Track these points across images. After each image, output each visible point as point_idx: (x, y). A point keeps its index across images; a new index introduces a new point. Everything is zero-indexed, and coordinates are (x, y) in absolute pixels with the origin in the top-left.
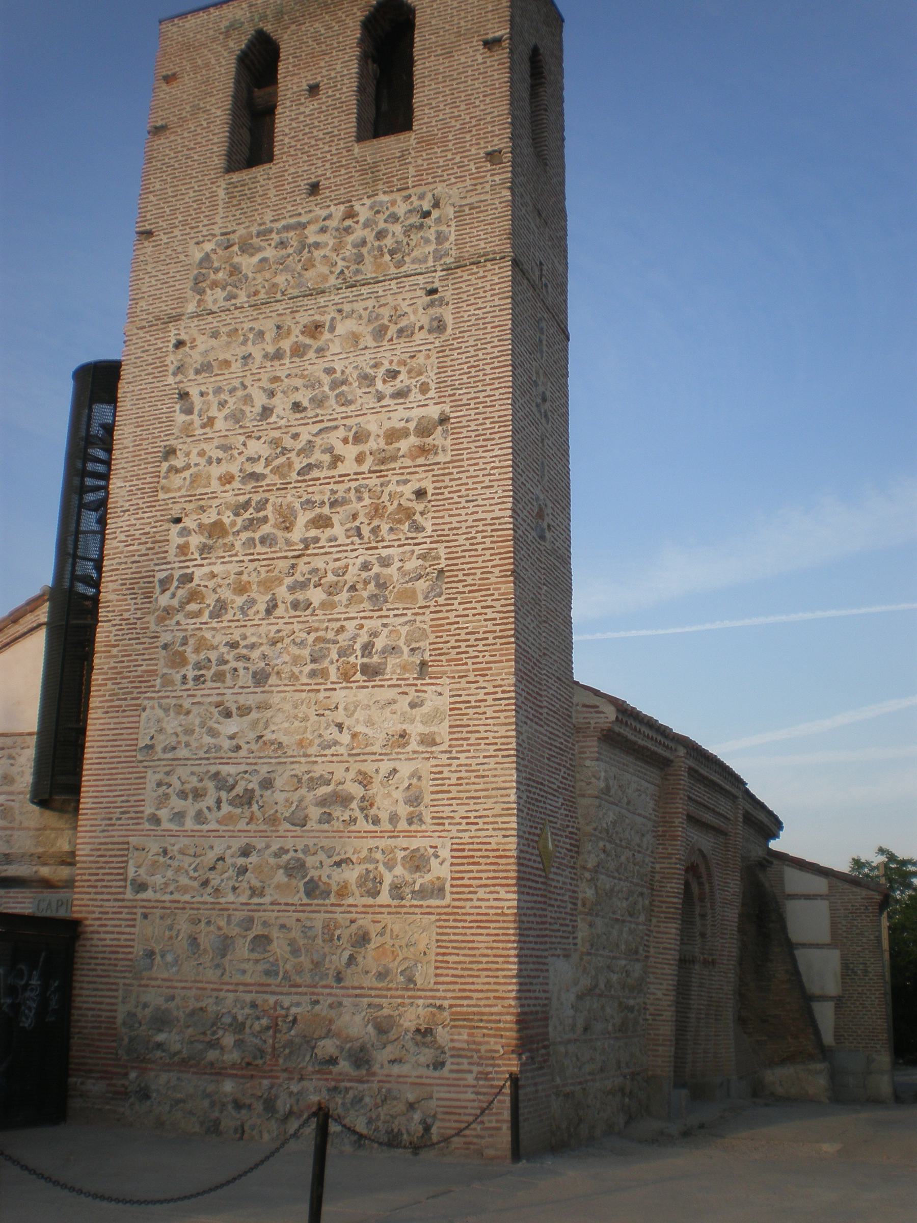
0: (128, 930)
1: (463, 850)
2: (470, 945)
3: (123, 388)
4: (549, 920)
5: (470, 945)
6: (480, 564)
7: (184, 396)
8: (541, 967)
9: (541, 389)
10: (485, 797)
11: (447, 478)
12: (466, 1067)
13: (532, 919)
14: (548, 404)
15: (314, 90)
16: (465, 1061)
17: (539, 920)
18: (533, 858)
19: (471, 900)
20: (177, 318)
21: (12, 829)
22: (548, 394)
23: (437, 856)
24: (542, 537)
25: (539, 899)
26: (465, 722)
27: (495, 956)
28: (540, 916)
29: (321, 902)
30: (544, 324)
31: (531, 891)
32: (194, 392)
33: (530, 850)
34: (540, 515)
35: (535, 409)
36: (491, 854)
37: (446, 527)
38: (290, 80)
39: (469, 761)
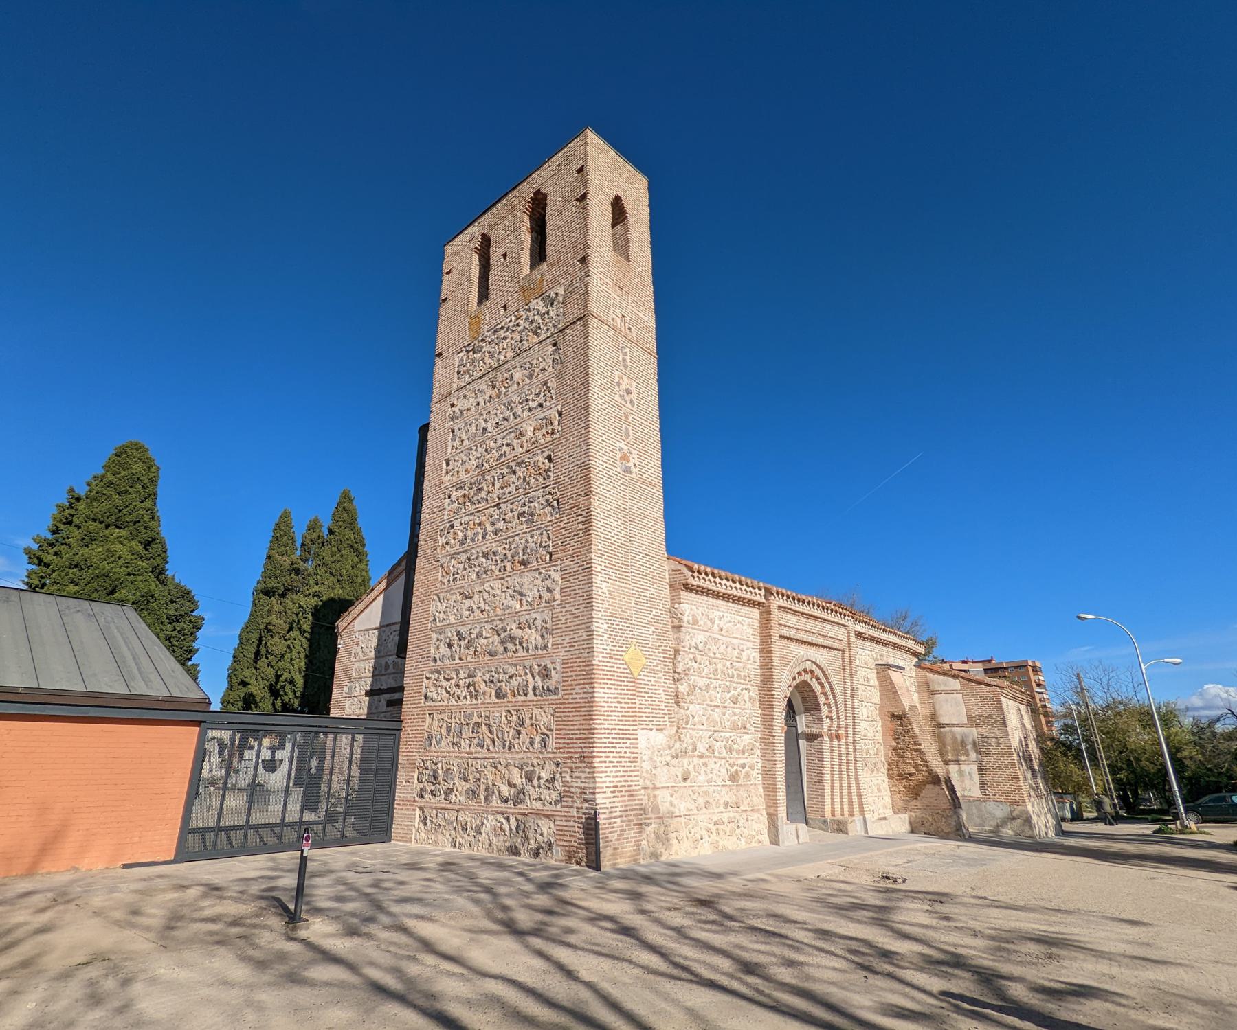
7: (453, 431)
15: (505, 256)
20: (449, 394)
32: (456, 429)
38: (495, 255)
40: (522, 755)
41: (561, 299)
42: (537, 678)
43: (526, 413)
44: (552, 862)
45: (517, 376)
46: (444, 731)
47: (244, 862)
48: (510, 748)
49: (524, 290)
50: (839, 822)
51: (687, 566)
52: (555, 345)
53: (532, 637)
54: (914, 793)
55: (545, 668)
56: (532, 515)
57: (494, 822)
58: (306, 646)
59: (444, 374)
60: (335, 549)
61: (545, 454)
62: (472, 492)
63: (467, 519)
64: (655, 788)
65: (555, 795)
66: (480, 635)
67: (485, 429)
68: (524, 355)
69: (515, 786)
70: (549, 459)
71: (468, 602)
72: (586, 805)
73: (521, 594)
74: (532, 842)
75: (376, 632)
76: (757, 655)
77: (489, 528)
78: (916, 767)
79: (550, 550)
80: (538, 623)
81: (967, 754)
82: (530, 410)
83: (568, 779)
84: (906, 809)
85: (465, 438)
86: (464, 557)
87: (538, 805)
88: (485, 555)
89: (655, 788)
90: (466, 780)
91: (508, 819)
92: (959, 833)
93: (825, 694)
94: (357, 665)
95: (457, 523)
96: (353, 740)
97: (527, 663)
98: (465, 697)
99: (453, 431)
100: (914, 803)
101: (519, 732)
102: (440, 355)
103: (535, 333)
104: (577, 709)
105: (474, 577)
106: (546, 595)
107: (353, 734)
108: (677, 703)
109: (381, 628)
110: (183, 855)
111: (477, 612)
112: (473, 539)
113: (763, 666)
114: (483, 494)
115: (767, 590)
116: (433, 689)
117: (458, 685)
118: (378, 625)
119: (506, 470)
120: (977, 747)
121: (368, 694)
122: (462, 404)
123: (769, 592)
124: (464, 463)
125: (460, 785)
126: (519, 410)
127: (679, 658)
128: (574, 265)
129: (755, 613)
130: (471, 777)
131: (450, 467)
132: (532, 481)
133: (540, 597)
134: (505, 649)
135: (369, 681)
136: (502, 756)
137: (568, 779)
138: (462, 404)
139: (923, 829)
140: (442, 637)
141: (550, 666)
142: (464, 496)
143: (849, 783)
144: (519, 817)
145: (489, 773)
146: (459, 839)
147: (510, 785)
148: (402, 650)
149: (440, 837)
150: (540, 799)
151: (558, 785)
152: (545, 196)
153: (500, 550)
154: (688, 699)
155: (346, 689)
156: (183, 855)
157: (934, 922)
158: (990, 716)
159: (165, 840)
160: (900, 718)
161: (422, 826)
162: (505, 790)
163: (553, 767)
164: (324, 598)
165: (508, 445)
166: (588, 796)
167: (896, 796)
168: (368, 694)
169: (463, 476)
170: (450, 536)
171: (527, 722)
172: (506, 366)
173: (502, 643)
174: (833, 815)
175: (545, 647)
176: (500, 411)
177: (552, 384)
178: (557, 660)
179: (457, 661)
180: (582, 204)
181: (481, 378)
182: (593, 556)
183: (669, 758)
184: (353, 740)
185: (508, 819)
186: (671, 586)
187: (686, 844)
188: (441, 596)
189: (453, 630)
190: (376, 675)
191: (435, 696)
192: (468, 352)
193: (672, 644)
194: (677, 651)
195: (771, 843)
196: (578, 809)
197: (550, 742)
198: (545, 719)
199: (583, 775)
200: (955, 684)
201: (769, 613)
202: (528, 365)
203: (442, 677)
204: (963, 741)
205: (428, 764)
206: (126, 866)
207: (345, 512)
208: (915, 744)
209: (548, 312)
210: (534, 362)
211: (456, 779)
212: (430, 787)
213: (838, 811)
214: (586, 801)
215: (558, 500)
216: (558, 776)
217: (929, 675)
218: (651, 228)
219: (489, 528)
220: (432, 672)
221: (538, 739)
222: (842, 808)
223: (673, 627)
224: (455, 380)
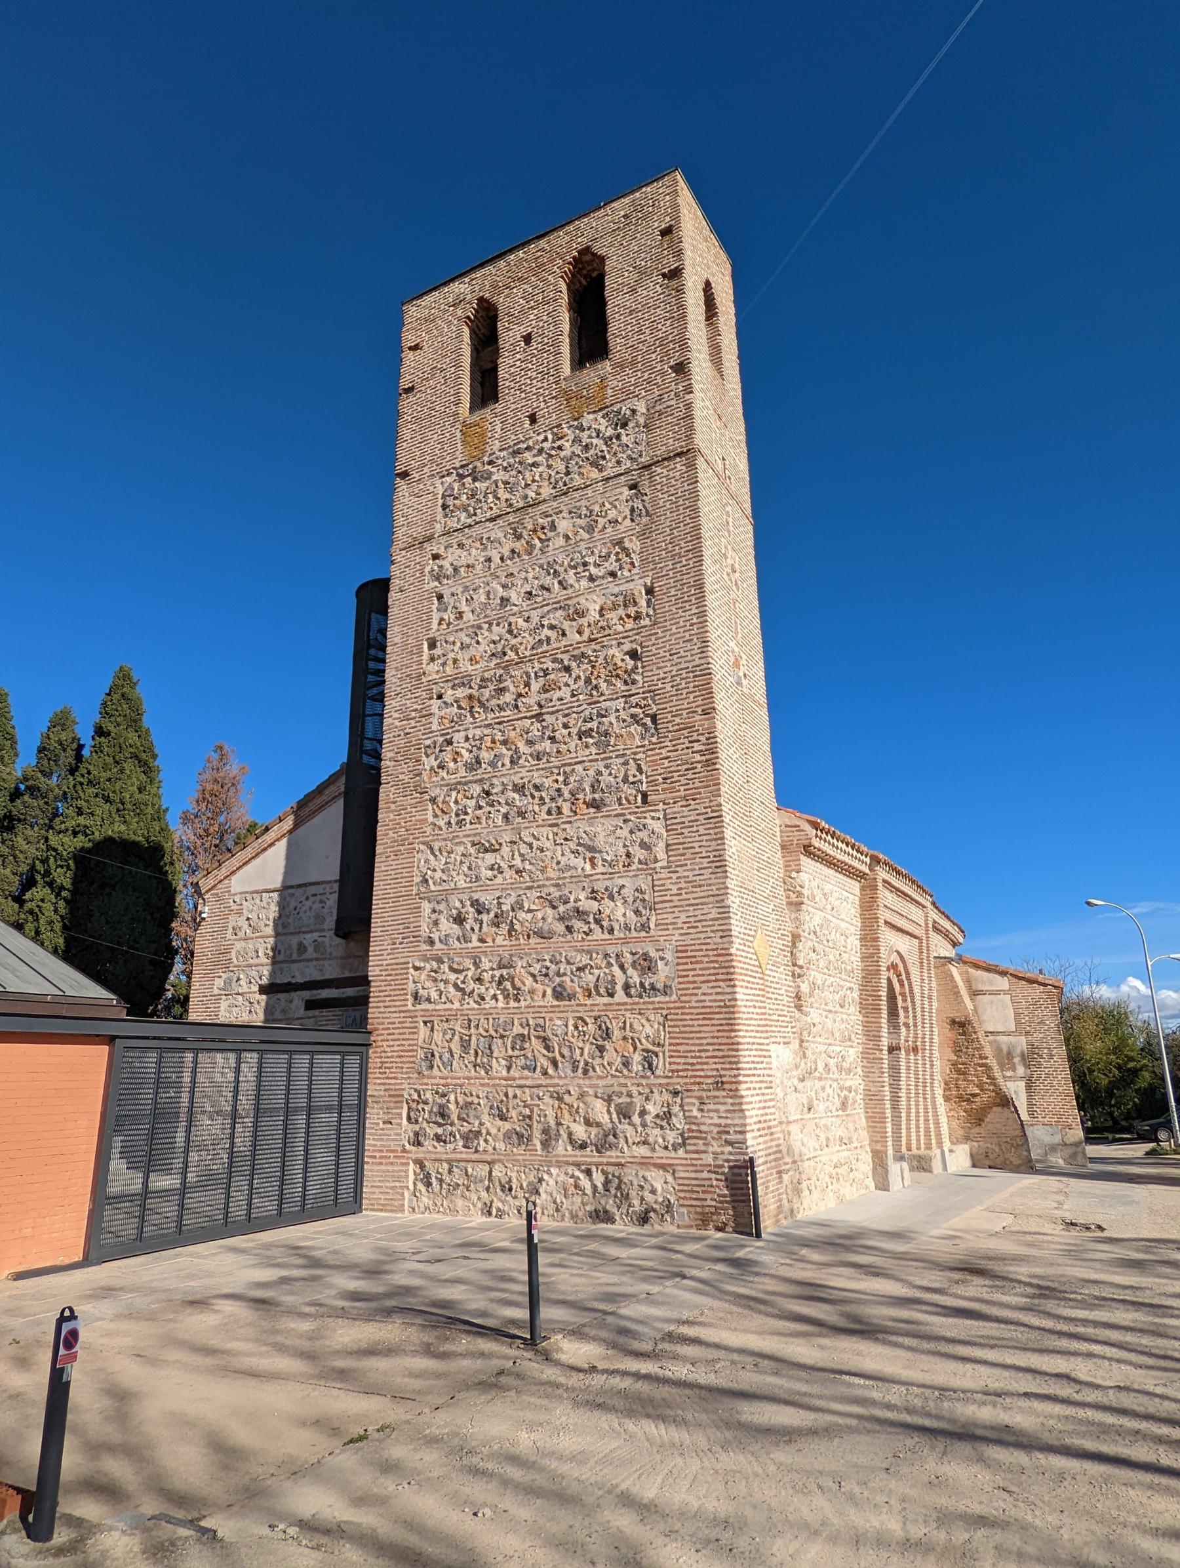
0: (411, 1036)
1: (687, 951)
2: (698, 1035)
3: (393, 596)
4: (768, 1011)
5: (698, 1035)
6: (686, 706)
7: (440, 597)
8: (764, 1053)
9: (730, 562)
10: (702, 904)
11: (653, 638)
12: (702, 1148)
13: (751, 1010)
14: (737, 575)
15: (528, 339)
16: (701, 1142)
17: (759, 1011)
18: (750, 956)
19: (696, 995)
20: (429, 539)
21: (324, 959)
22: (737, 566)
23: (662, 959)
24: (739, 683)
25: (757, 992)
26: (682, 841)
27: (720, 1044)
28: (760, 1008)
29: (567, 1003)
30: (729, 509)
31: (750, 985)
32: (446, 593)
33: (746, 949)
34: (737, 665)
35: (725, 577)
36: (711, 953)
37: (655, 678)
38: (509, 335)
39: (686, 874)
40: (609, 1081)
41: (642, 420)
42: (630, 971)
43: (584, 583)
44: (673, 1229)
45: (563, 525)
46: (455, 1046)
47: (197, 1256)
48: (585, 1072)
49: (568, 396)
50: (920, 1158)
51: (809, 821)
52: (633, 487)
53: (618, 912)
54: (977, 1118)
55: (646, 957)
56: (606, 734)
57: (562, 1178)
58: (63, 911)
59: (412, 506)
60: (110, 760)
61: (627, 647)
62: (486, 693)
63: (478, 732)
64: (789, 1122)
65: (672, 1137)
66: (518, 906)
67: (505, 601)
68: (577, 495)
69: (598, 1125)
70: (633, 655)
71: (490, 858)
72: (730, 1149)
73: (591, 849)
74: (636, 1202)
75: (275, 895)
76: (858, 943)
77: (523, 748)
78: (980, 1086)
79: (644, 787)
80: (628, 892)
81: (1014, 1069)
82: (592, 579)
83: (695, 1113)
84: (967, 1139)
85: (464, 607)
86: (476, 789)
87: (643, 1151)
88: (519, 789)
89: (789, 1122)
90: (503, 1118)
91: (588, 1173)
92: (1029, 1167)
93: (903, 995)
94: (239, 946)
95: (458, 737)
96: (239, 1062)
97: (611, 950)
98: (495, 997)
99: (440, 597)
100: (977, 1130)
101: (601, 1049)
102: (404, 475)
103: (595, 464)
104: (707, 1016)
105: (499, 820)
106: (639, 853)
107: (239, 1051)
108: (799, 1008)
109: (286, 890)
110: (96, 1252)
111: (508, 873)
112: (493, 764)
113: (864, 958)
114: (508, 698)
115: (873, 858)
116: (428, 984)
117: (479, 980)
118: (278, 884)
119: (550, 665)
120: (1027, 1060)
121: (263, 990)
122: (452, 557)
123: (875, 860)
124: (463, 647)
125: (491, 1125)
126: (571, 578)
127: (800, 946)
128: (663, 373)
129: (855, 886)
130: (513, 1113)
131: (438, 651)
132: (604, 685)
133: (628, 855)
134: (569, 929)
135: (266, 971)
136: (565, 1078)
137: (695, 1113)
138: (452, 557)
139: (988, 1162)
140: (442, 907)
141: (653, 954)
142: (470, 697)
143: (926, 1108)
144: (610, 1169)
145: (548, 1107)
146: (497, 1204)
147: (588, 1123)
148: (354, 921)
149: (460, 1203)
150: (645, 1143)
151: (678, 1122)
152: (602, 259)
153: (547, 782)
154: (810, 1000)
155: (219, 983)
156: (96, 1252)
157: (490, 1283)
158: (1042, 1022)
159: (68, 1232)
160: (962, 1025)
161: (421, 1186)
162: (580, 1131)
163: (667, 1097)
164: (97, 836)
165: (552, 627)
166: (733, 1136)
167: (955, 1123)
168: (263, 990)
169: (466, 667)
170: (447, 757)
171: (617, 1034)
172: (543, 507)
173: (562, 919)
174: (909, 1149)
175: (645, 927)
176: (534, 577)
177: (633, 545)
178: (665, 947)
179: (475, 943)
180: (674, 283)
181: (491, 520)
182: (722, 800)
183: (796, 1081)
184: (239, 1062)
185: (588, 1173)
186: (783, 847)
187: (816, 1195)
188: (436, 847)
189: (465, 897)
190: (278, 958)
191: (434, 995)
192: (461, 477)
193: (789, 926)
194: (796, 938)
195: (877, 1188)
196: (716, 1153)
197: (660, 1063)
198: (647, 1029)
199: (722, 1108)
200: (1003, 983)
201: (875, 888)
202: (584, 511)
203: (445, 967)
204: (1009, 1053)
205: (429, 1095)
206: (19, 1276)
207: (121, 703)
208: (981, 1057)
209: (618, 437)
210: (597, 508)
211: (485, 1118)
212: (432, 1130)
213: (914, 1146)
214: (729, 1143)
215: (654, 718)
216: (676, 1109)
217: (972, 971)
218: (738, 334)
219: (523, 748)
220: (426, 959)
221: (637, 1058)
222: (918, 1140)
223: (790, 904)
224: (439, 517)
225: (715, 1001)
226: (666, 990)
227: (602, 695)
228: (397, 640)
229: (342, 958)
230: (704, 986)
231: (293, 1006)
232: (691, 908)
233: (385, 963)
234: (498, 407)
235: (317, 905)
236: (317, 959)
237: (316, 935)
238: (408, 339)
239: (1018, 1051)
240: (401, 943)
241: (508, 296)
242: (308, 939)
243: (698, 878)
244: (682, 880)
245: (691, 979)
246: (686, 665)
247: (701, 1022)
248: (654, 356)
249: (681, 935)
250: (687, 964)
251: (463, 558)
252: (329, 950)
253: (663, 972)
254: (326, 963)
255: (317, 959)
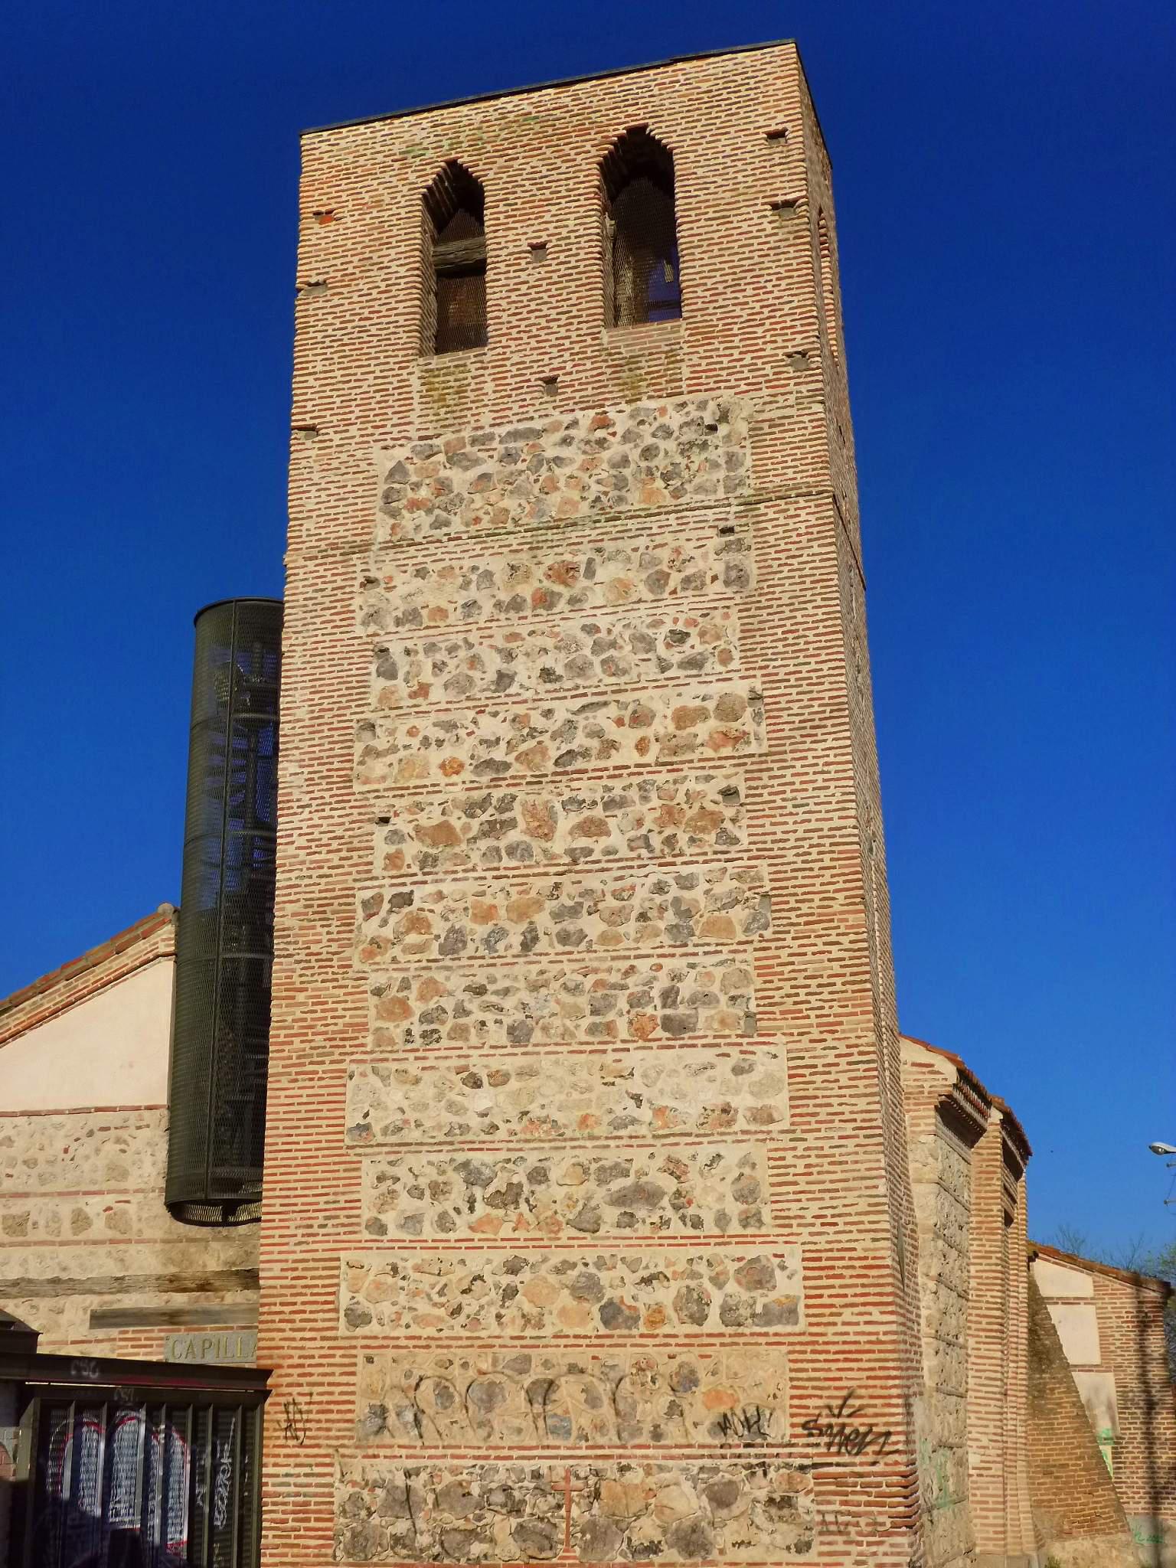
1: (819, 1259)
19: (835, 1324)
21: (129, 1241)
23: (783, 1268)
29: (625, 1332)
32: (396, 649)
36: (857, 1263)
39: (819, 1143)
225: (863, 1333)
226: (789, 1313)
227: (681, 855)
228: (301, 713)
229: (165, 1241)
230: (847, 1311)
231: (64, 1319)
232: (827, 1195)
233: (291, 1257)
234: (489, 354)
235: (111, 1148)
236: (112, 1242)
237: (109, 1200)
238: (311, 199)
239: (1103, 1398)
240: (321, 1226)
241: (503, 170)
242: (94, 1206)
243: (836, 1151)
244: (813, 1153)
245: (826, 1301)
246: (819, 825)
247: (841, 1365)
248: (760, 330)
249: (811, 1234)
250: (820, 1278)
251: (430, 595)
252: (136, 1226)
253: (788, 1286)
254: (133, 1248)
255: (112, 1242)
